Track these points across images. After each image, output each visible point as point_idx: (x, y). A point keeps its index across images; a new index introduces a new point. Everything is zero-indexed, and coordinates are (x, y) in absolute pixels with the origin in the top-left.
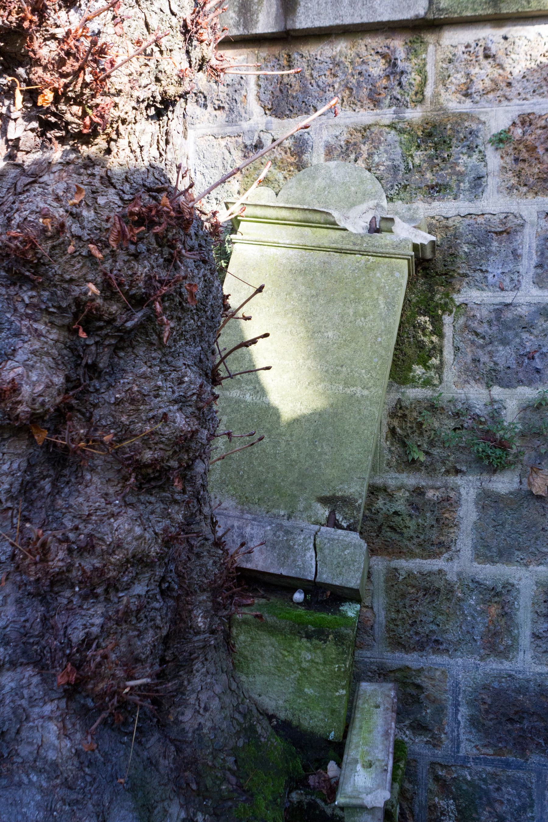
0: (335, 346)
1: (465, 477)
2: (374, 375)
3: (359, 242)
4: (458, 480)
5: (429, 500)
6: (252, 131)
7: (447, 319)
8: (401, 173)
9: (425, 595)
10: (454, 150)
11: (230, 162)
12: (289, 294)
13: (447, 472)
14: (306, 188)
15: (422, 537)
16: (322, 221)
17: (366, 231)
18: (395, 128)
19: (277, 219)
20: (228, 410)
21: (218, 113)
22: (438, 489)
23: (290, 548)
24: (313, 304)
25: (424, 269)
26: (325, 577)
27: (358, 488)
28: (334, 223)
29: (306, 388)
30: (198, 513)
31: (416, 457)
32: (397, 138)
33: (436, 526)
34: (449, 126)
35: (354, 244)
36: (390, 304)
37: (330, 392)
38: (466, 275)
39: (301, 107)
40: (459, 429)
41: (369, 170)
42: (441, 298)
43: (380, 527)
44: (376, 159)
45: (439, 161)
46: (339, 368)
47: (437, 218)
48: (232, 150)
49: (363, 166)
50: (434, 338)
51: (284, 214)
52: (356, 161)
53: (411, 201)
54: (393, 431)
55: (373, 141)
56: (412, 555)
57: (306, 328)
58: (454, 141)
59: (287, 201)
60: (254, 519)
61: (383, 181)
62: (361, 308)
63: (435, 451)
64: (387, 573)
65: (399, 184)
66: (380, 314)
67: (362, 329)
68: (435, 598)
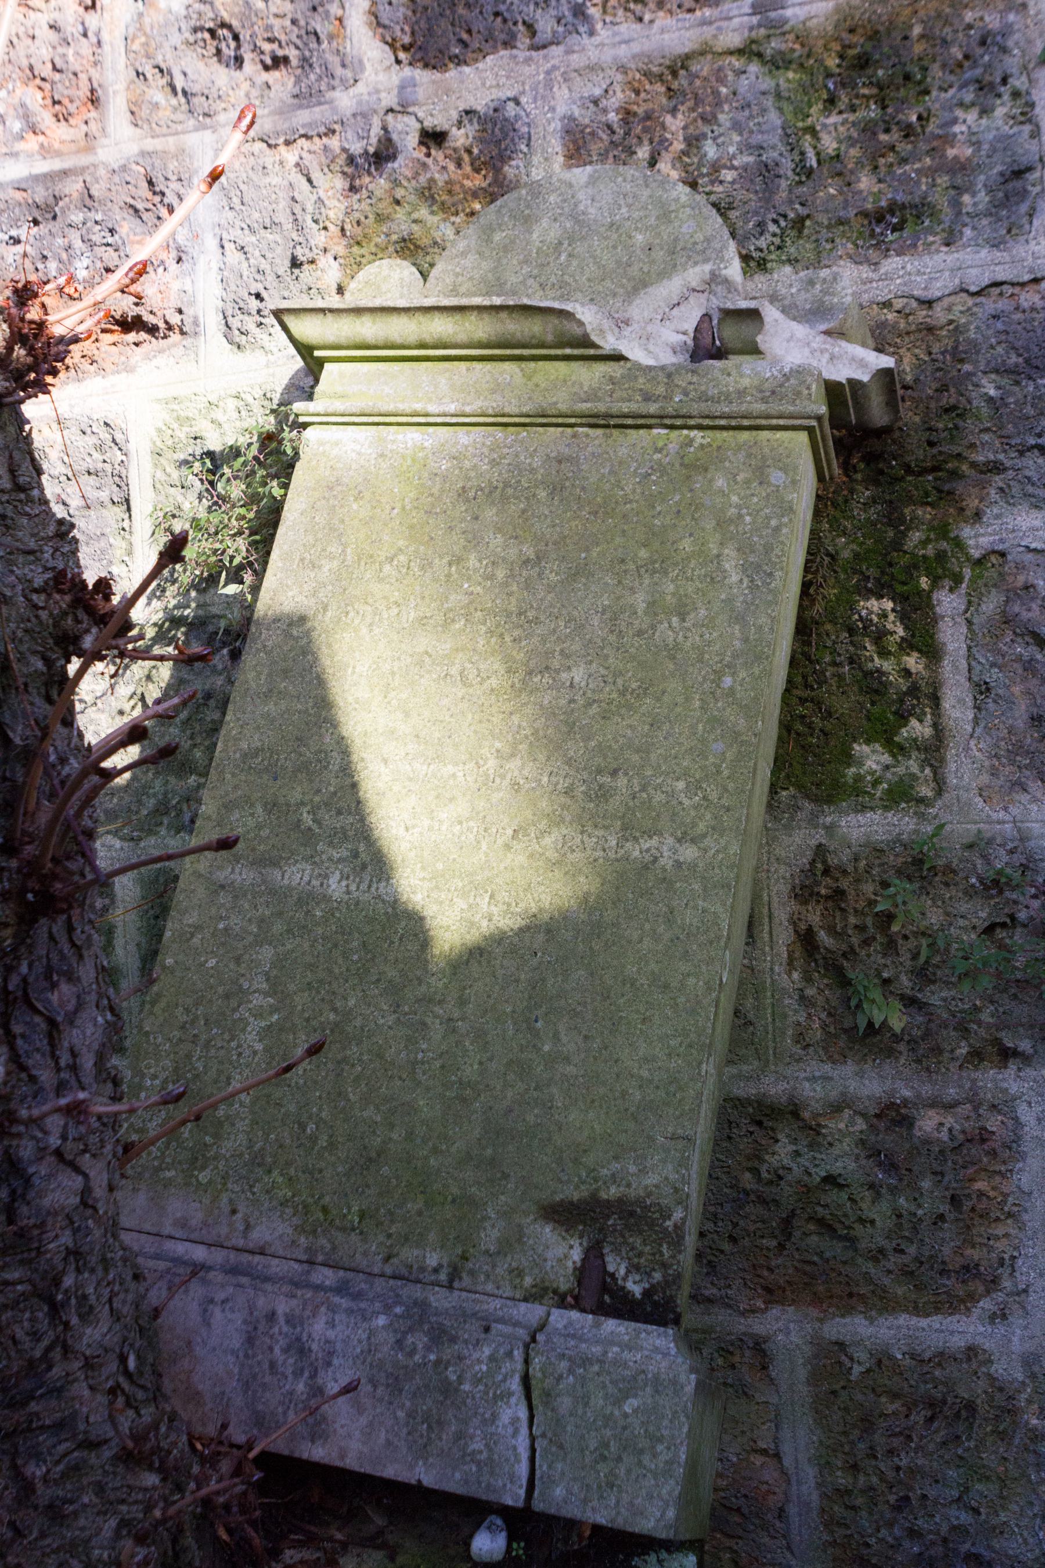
0: (594, 709)
1: (1029, 1072)
2: (714, 796)
3: (661, 390)
4: (1011, 1080)
5: (927, 1142)
6: (364, 115)
7: (948, 603)
8: (784, 184)
9: (931, 1420)
10: (936, 100)
11: (310, 208)
12: (458, 560)
13: (976, 1056)
14: (506, 249)
15: (912, 1250)
16: (550, 338)
17: (682, 359)
18: (760, 55)
19: (423, 346)
20: (278, 927)
21: (273, 76)
22: (950, 1106)
23: (448, 1390)
24: (528, 585)
25: (870, 458)
26: (560, 1497)
27: (669, 1171)
28: (585, 342)
29: (508, 847)
30: (57, 1354)
31: (878, 1019)
32: (767, 83)
33: (950, 1216)
34: (917, 30)
35: (647, 398)
36: (759, 571)
37: (577, 856)
38: (996, 468)
39: (490, 31)
40: (1003, 925)
41: (693, 185)
42: (925, 543)
43: (787, 1222)
44: (711, 151)
45: (895, 136)
46: (606, 779)
47: (898, 304)
48: (316, 175)
49: (675, 175)
50: (913, 662)
51: (440, 327)
52: (653, 163)
53: (817, 263)
54: (807, 939)
55: (698, 100)
56: (888, 1305)
57: (507, 659)
58: (936, 71)
59: (454, 291)
60: (341, 1289)
61: (733, 214)
62: (671, 588)
63: (935, 997)
64: (816, 1356)
65: (780, 219)
66: (729, 601)
67: (673, 652)
68: (961, 1428)
